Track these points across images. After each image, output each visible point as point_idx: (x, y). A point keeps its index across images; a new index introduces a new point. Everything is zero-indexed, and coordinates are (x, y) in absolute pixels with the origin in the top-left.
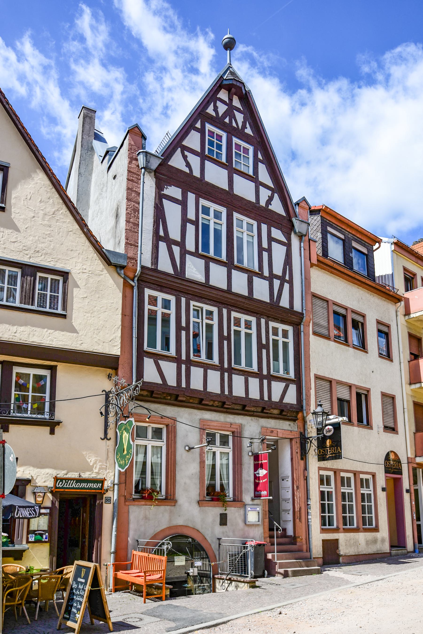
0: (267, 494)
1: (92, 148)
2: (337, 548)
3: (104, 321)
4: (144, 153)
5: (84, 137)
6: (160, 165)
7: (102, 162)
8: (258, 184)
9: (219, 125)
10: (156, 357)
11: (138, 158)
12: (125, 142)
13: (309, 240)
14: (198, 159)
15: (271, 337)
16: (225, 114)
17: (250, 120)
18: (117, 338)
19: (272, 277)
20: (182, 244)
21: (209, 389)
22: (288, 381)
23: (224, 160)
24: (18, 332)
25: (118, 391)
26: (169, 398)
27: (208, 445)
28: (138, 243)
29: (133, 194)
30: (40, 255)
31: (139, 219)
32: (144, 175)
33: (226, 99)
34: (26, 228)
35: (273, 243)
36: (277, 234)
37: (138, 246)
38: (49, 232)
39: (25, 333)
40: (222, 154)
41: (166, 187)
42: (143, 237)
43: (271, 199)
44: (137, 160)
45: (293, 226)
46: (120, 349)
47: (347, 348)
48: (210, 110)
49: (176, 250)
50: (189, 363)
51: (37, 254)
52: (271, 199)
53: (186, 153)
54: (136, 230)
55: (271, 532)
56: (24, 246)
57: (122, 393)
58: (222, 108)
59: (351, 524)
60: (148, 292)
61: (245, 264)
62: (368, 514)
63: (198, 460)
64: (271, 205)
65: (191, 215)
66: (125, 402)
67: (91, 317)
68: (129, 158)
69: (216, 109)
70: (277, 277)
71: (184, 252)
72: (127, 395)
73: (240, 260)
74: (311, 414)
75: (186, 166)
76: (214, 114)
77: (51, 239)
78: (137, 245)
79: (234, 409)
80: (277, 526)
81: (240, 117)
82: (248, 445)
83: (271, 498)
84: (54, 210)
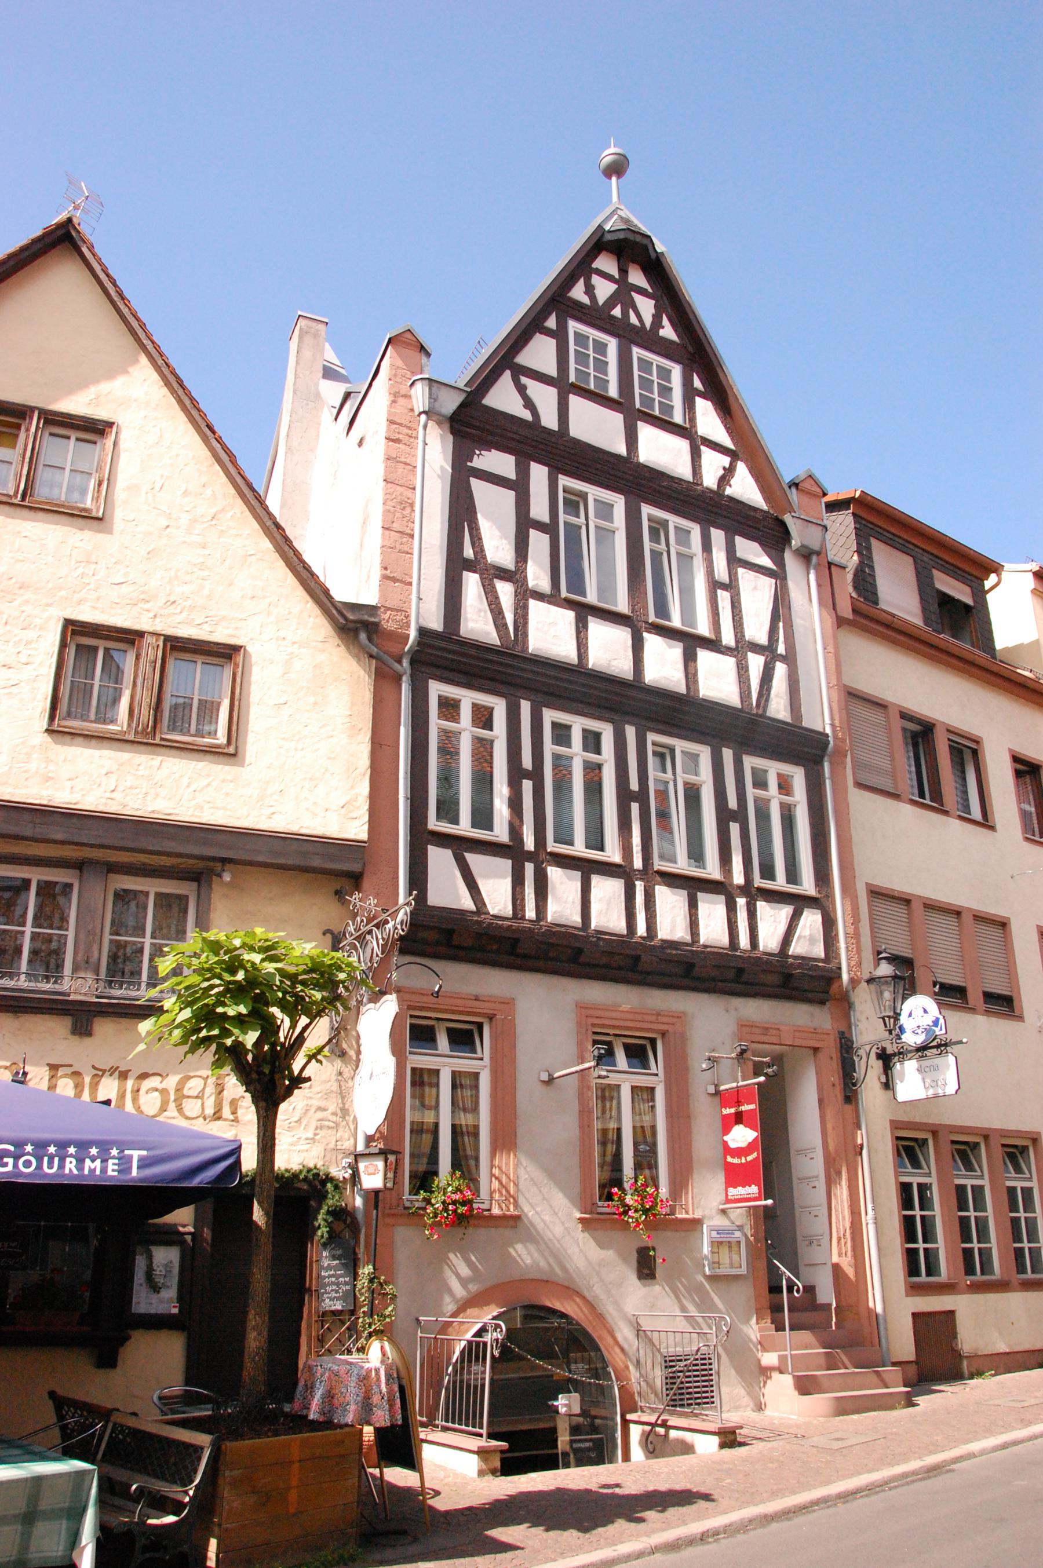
0: (759, 1193)
1: (318, 395)
2: (954, 1334)
3: (329, 758)
4: (424, 382)
5: (301, 375)
6: (462, 405)
7: (336, 419)
8: (697, 443)
9: (598, 322)
10: (459, 845)
11: (413, 391)
12: (383, 364)
13: (830, 564)
14: (552, 393)
15: (751, 792)
16: (612, 302)
17: (669, 310)
18: (360, 798)
19: (741, 649)
20: (515, 576)
21: (596, 922)
22: (800, 902)
23: (613, 392)
24: (121, 788)
25: (360, 929)
26: (495, 947)
27: (598, 1064)
28: (411, 577)
29: (400, 471)
30: (179, 611)
31: (413, 523)
32: (425, 427)
33: (615, 273)
34: (149, 553)
35: (741, 571)
36: (749, 549)
37: (410, 584)
38: (201, 560)
39: (137, 791)
40: (608, 381)
41: (477, 452)
42: (423, 563)
43: (728, 473)
44: (408, 397)
45: (787, 532)
46: (366, 827)
47: (944, 818)
48: (578, 293)
49: (505, 591)
50: (542, 857)
51: (171, 609)
52: (728, 473)
53: (524, 380)
54: (406, 549)
55: (775, 1296)
56: (143, 592)
57: (370, 932)
58: (604, 290)
59: (986, 1268)
60: (436, 689)
61: (676, 622)
62: (975, 1211)
63: (575, 1106)
64: (730, 486)
65: (539, 510)
66: (377, 956)
67: (296, 749)
68: (390, 394)
69: (590, 290)
70: (756, 648)
71: (524, 594)
72: (380, 936)
73: (662, 609)
74: (864, 984)
75: (525, 407)
76: (585, 300)
77: (206, 573)
78: (410, 580)
79: (664, 974)
80: (789, 1279)
81: (646, 307)
82: (704, 1066)
83: (770, 1202)
84: (214, 510)
